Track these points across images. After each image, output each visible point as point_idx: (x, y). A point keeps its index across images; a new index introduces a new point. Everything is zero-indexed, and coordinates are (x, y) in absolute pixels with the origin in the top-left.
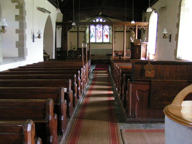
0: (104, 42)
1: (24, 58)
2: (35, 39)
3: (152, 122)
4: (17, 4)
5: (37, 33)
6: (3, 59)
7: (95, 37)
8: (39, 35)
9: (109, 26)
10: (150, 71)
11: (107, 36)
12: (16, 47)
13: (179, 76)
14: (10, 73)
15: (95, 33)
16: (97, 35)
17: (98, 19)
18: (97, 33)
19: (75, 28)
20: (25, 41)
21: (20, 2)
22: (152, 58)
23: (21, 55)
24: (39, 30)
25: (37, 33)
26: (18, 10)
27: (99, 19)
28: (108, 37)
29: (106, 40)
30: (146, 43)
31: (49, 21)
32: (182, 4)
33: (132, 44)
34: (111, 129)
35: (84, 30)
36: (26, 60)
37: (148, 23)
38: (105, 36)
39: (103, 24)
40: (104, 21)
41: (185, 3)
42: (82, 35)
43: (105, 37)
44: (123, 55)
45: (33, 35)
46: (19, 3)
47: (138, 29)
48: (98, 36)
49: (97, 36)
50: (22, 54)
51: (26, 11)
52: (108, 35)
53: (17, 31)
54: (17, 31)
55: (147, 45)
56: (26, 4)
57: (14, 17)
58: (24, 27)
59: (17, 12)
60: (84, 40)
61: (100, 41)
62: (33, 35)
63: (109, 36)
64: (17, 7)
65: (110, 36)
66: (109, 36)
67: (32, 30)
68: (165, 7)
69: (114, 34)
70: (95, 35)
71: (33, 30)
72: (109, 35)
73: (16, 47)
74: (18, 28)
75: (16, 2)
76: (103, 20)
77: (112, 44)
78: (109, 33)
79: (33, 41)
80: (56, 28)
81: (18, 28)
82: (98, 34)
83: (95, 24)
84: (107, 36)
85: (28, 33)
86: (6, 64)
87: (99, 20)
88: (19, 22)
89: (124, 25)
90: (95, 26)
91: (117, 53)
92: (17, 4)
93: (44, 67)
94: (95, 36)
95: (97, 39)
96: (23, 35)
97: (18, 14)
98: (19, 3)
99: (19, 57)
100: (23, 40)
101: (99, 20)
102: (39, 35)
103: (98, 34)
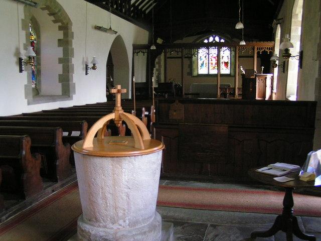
0: (210, 73)
1: (69, 96)
2: (89, 71)
3: (182, 179)
4: (60, 24)
5: (91, 63)
6: (33, 98)
7: (207, 66)
8: (94, 65)
9: (230, 48)
10: (175, 111)
11: (226, 64)
12: (59, 82)
13: (292, 128)
14: (44, 115)
15: (207, 60)
16: (210, 62)
17: (213, 37)
18: (210, 60)
19: (144, 53)
20: (70, 74)
21: (64, 21)
22: (293, 98)
23: (65, 93)
24: (94, 58)
25: (91, 63)
26: (62, 32)
27: (214, 37)
28: (228, 66)
29: (225, 71)
30: (264, 74)
31: (118, 44)
32: (293, 15)
33: (243, 75)
34: (266, 218)
35: (252, 55)
36: (72, 99)
37: (273, 42)
38: (224, 64)
39: (219, 46)
40: (222, 41)
41: (297, 13)
42: (186, 61)
43: (222, 66)
44: (234, 94)
45: (87, 66)
46: (63, 23)
47: (258, 53)
48: (212, 64)
49: (210, 64)
50: (67, 92)
51: (73, 33)
52: (228, 63)
53: (61, 61)
54: (61, 61)
55: (266, 78)
56: (73, 24)
57: (56, 43)
58: (70, 54)
59: (60, 35)
60: (188, 70)
61: (215, 72)
62: (87, 66)
63: (229, 64)
64: (60, 28)
65: (230, 63)
66: (229, 64)
67: (83, 58)
68: (282, 19)
69: (237, 61)
70: (207, 62)
71: (87, 59)
72: (229, 62)
73: (59, 82)
74: (61, 56)
75: (59, 22)
76: (220, 39)
77: (235, 76)
78: (229, 60)
79: (87, 74)
80: (133, 53)
81: (61, 56)
82: (212, 60)
83: (208, 46)
84: (226, 64)
85: (77, 63)
86: (39, 103)
87: (214, 40)
88: (63, 48)
89: (235, 47)
90: (208, 48)
91: (224, 90)
92: (60, 24)
93: (107, 109)
94: (207, 64)
95: (210, 69)
96: (68, 66)
97: (61, 37)
98: (63, 23)
99: (63, 95)
100: (69, 73)
101: (214, 40)
102: (94, 65)
103: (212, 60)
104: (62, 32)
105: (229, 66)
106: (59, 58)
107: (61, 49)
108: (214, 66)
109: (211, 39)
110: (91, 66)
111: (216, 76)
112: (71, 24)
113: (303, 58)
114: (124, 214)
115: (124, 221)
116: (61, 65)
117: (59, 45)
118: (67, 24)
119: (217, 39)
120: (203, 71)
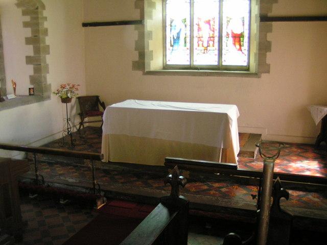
7: (188, 45)
11: (238, 38)
16: (196, 33)
18: (196, 28)
38: (231, 39)
48: (199, 38)
66: (246, 39)
70: (188, 34)
72: (246, 35)
84: (238, 38)
94: (188, 40)
95: (195, 52)
97: (31, 54)
108: (205, 45)
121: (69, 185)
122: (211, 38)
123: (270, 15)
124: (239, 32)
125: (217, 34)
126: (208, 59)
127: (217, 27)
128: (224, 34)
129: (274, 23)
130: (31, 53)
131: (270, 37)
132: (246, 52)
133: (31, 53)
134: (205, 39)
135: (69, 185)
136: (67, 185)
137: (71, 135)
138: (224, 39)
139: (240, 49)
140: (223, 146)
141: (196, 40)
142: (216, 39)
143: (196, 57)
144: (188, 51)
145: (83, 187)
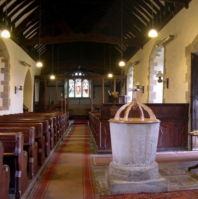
0: (76, 97)
1: (7, 108)
4: (3, 58)
7: (74, 92)
11: (86, 91)
15: (74, 88)
16: (76, 89)
18: (76, 88)
23: (5, 105)
29: (86, 95)
38: (85, 91)
39: (83, 78)
46: (5, 57)
47: (116, 82)
48: (77, 91)
52: (87, 90)
53: (2, 83)
54: (2, 83)
59: (2, 65)
64: (3, 61)
66: (88, 91)
70: (74, 89)
72: (88, 89)
76: (82, 74)
78: (88, 88)
79: (15, 93)
80: (35, 82)
81: (3, 79)
83: (74, 78)
84: (86, 91)
86: (190, 67)
87: (78, 74)
92: (3, 58)
94: (74, 91)
95: (76, 94)
97: (3, 67)
98: (5, 57)
101: (78, 74)
104: (4, 63)
105: (88, 92)
106: (1, 81)
107: (3, 75)
108: (78, 92)
109: (76, 74)
110: (19, 87)
111: (79, 98)
112: (10, 59)
113: (169, 82)
114: (149, 157)
115: (148, 161)
116: (3, 86)
117: (2, 72)
118: (8, 58)
119: (80, 74)
120: (71, 95)
121: (90, 168)
122: (80, 90)
123: (95, 85)
124: (87, 89)
125: (81, 89)
126: (79, 96)
127: (81, 88)
128: (83, 89)
129: (96, 87)
130: (3, 66)
131: (95, 90)
132: (88, 94)
133: (3, 66)
134: (78, 91)
135: (90, 168)
136: (90, 167)
137: (89, 154)
138: (83, 91)
139: (87, 93)
140: (53, 125)
141: (76, 91)
142: (81, 91)
143: (76, 95)
144: (74, 94)
145: (83, 188)
